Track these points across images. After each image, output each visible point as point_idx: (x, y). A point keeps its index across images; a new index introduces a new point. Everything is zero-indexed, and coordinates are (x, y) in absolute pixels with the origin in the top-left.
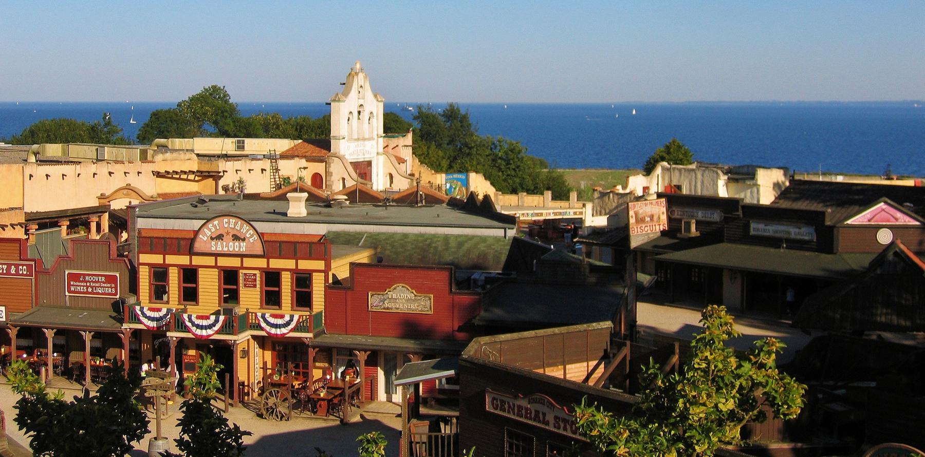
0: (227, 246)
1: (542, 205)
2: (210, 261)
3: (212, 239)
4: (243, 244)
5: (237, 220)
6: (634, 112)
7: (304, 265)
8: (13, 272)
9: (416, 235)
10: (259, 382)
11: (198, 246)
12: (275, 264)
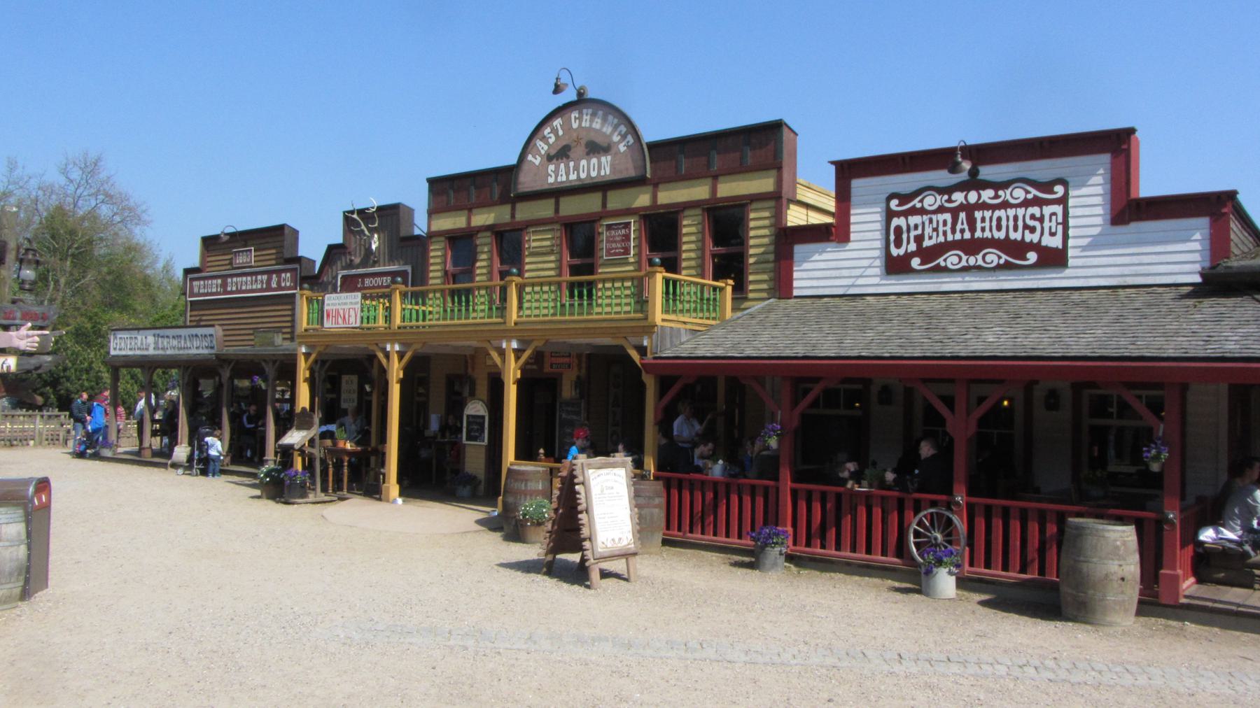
0: (576, 168)
1: (1058, 209)
2: (544, 209)
3: (550, 158)
4: (606, 160)
5: (539, 135)
6: (1006, 403)
7: (730, 188)
8: (274, 285)
9: (264, 432)
10: (642, 350)
11: (527, 182)
12: (670, 196)
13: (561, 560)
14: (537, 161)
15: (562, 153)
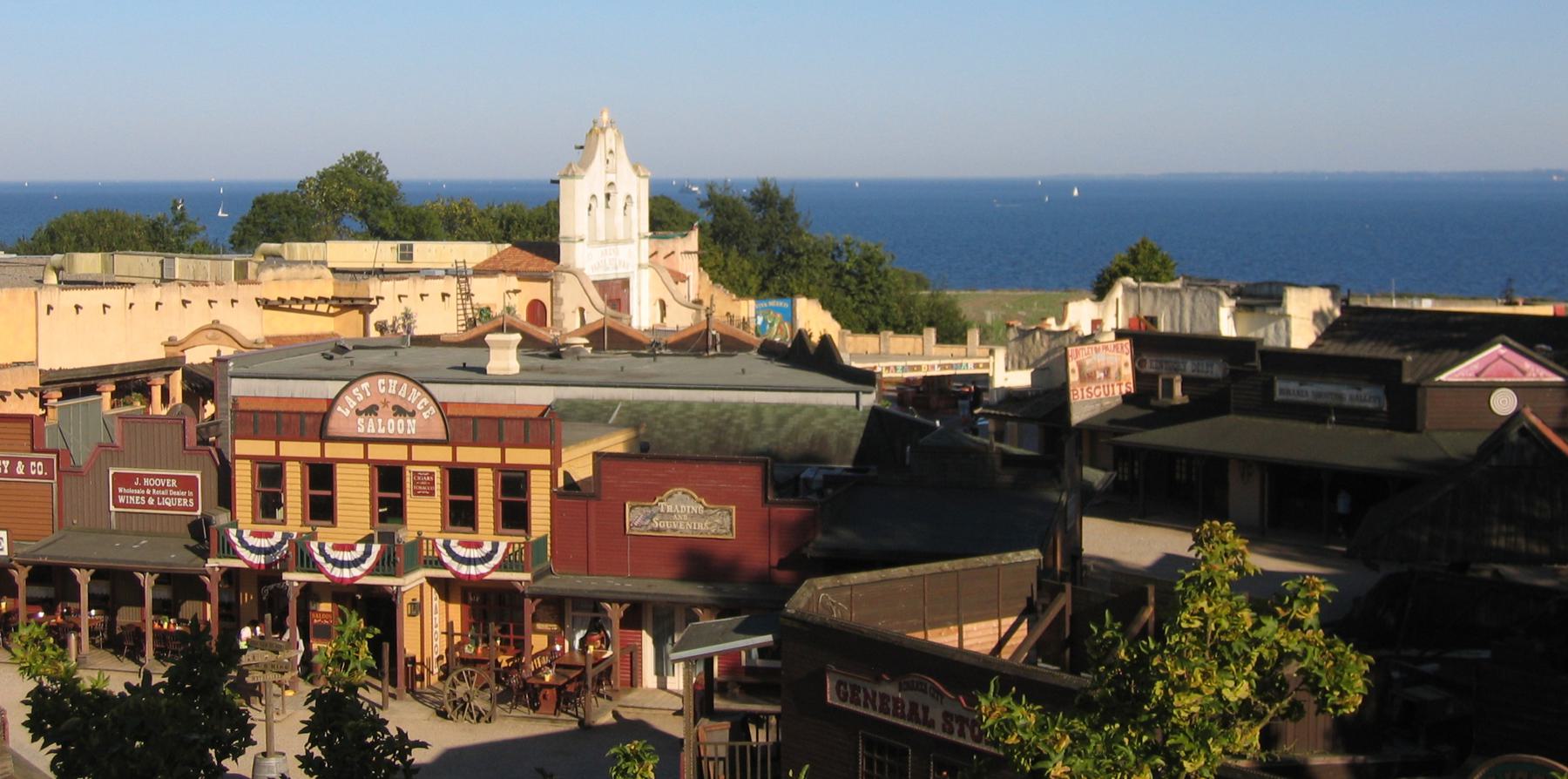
0: (384, 425)
2: (356, 451)
3: (359, 413)
4: (411, 422)
7: (516, 456)
11: (335, 426)
12: (467, 455)
13: (774, 703)
14: (347, 413)
15: (372, 410)
